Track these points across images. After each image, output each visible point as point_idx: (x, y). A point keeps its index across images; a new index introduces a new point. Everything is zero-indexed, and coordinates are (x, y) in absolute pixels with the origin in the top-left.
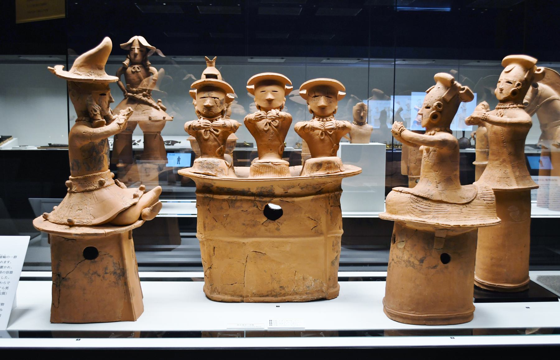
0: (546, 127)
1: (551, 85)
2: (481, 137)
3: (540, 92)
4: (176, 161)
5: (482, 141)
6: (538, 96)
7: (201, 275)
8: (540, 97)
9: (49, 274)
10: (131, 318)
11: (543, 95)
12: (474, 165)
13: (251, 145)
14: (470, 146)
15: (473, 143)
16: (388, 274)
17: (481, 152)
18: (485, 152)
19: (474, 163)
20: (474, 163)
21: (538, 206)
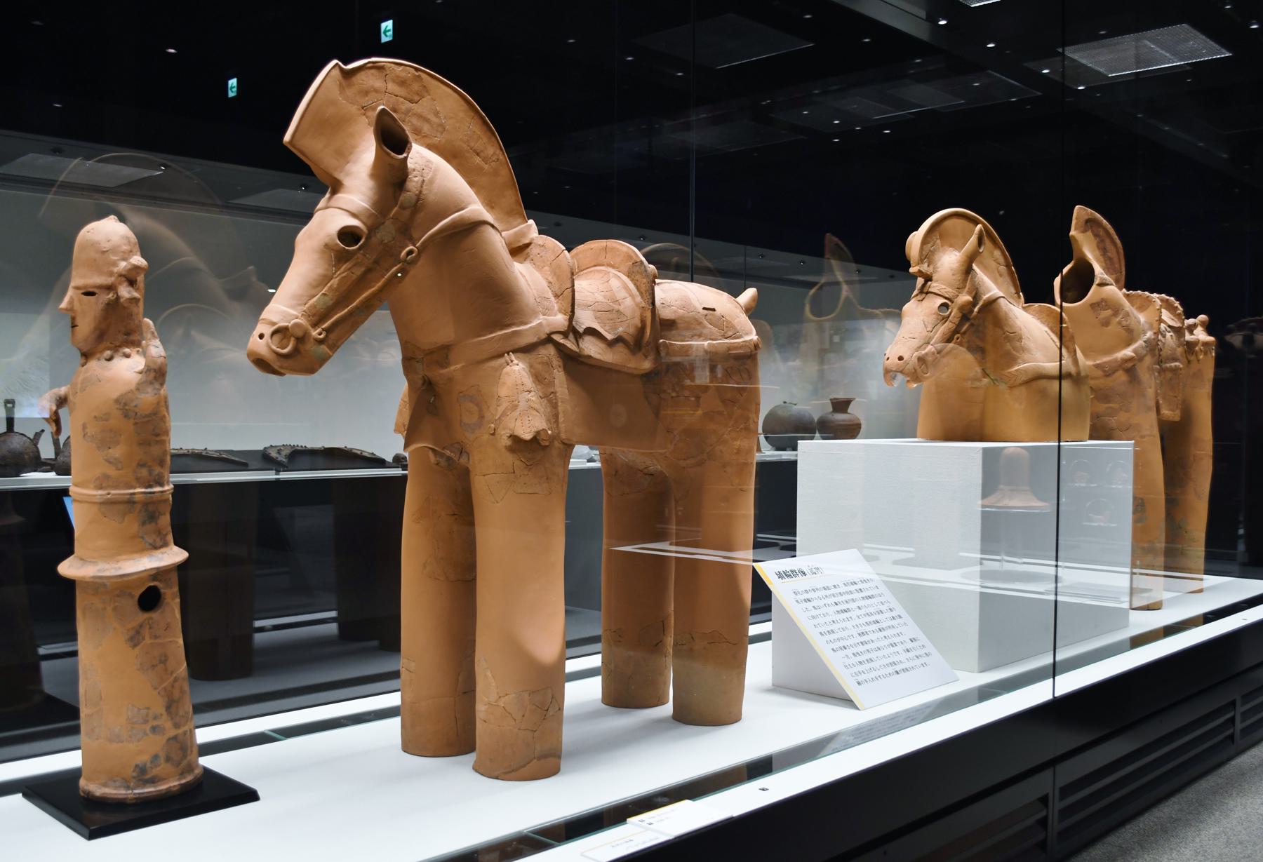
0: (444, 363)
1: (451, 155)
2: (103, 418)
3: (413, 182)
4: (79, 321)
5: (106, 440)
6: (405, 197)
7: (394, 700)
8: (418, 204)
9: (333, 614)
10: (985, 450)
11: (431, 196)
12: (70, 584)
13: (1090, 224)
14: (38, 464)
15: (46, 450)
16: (773, 627)
17: (109, 503)
18: (130, 502)
19: (67, 569)
20: (67, 569)
21: (413, 744)
